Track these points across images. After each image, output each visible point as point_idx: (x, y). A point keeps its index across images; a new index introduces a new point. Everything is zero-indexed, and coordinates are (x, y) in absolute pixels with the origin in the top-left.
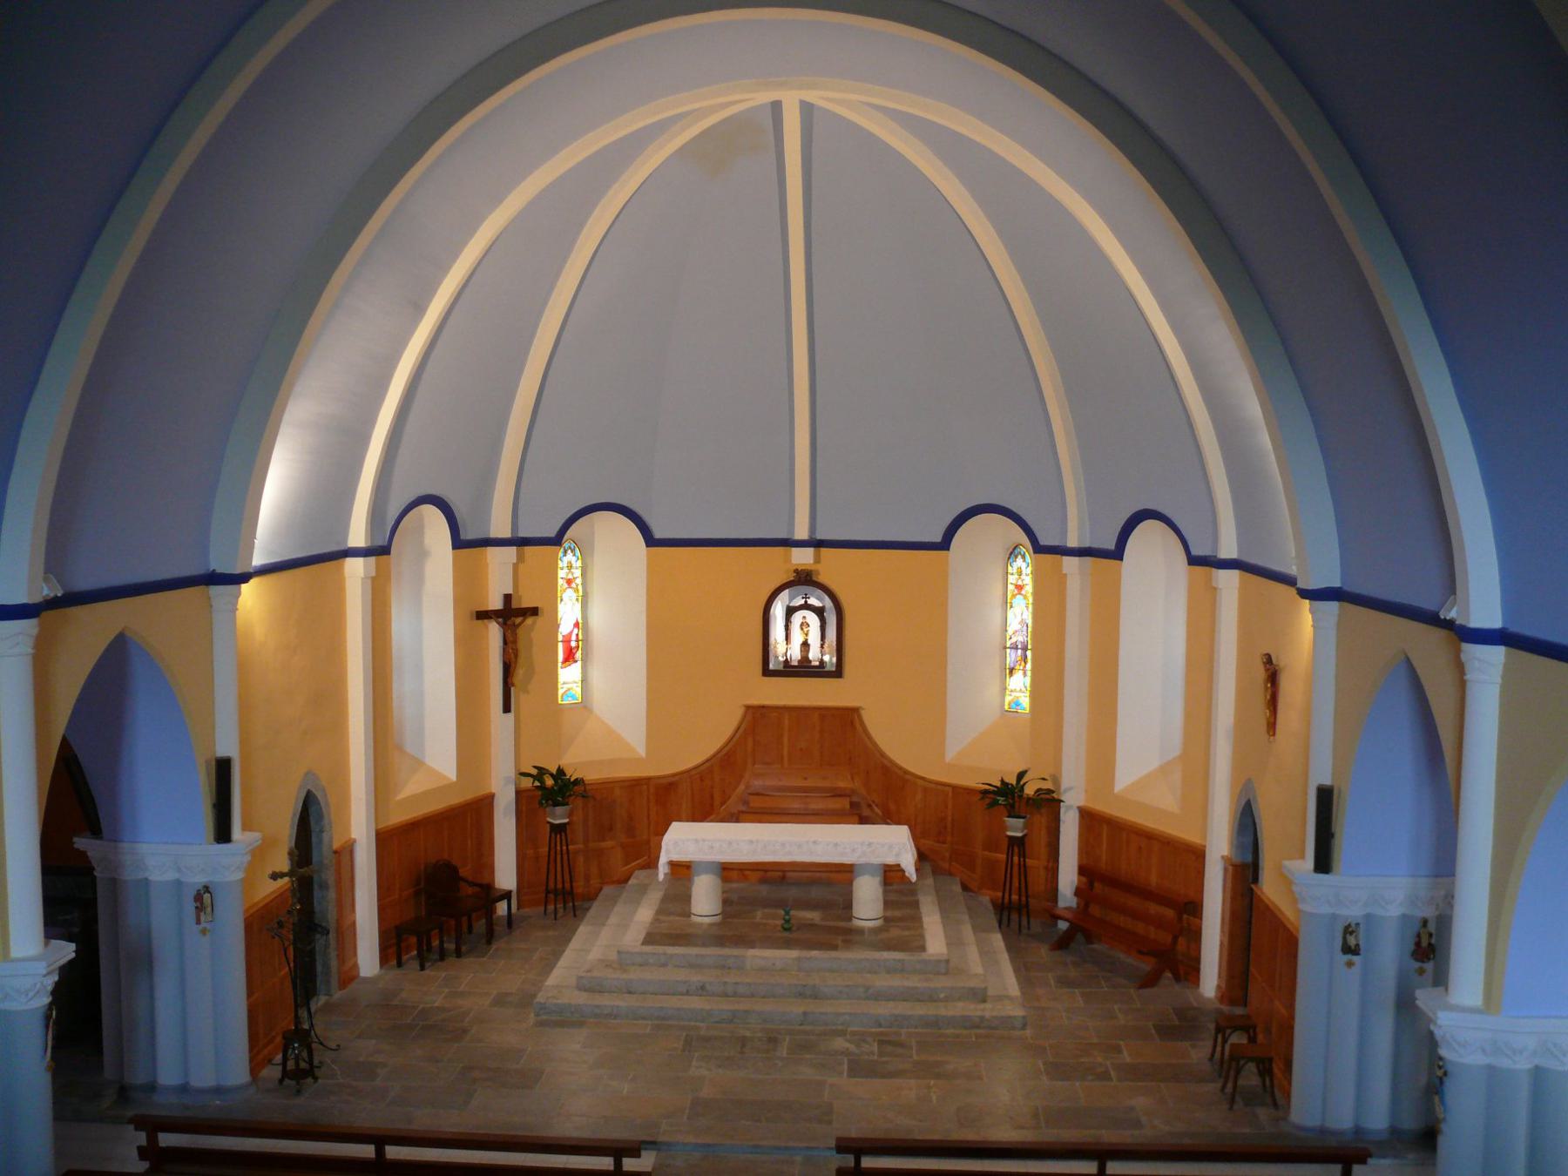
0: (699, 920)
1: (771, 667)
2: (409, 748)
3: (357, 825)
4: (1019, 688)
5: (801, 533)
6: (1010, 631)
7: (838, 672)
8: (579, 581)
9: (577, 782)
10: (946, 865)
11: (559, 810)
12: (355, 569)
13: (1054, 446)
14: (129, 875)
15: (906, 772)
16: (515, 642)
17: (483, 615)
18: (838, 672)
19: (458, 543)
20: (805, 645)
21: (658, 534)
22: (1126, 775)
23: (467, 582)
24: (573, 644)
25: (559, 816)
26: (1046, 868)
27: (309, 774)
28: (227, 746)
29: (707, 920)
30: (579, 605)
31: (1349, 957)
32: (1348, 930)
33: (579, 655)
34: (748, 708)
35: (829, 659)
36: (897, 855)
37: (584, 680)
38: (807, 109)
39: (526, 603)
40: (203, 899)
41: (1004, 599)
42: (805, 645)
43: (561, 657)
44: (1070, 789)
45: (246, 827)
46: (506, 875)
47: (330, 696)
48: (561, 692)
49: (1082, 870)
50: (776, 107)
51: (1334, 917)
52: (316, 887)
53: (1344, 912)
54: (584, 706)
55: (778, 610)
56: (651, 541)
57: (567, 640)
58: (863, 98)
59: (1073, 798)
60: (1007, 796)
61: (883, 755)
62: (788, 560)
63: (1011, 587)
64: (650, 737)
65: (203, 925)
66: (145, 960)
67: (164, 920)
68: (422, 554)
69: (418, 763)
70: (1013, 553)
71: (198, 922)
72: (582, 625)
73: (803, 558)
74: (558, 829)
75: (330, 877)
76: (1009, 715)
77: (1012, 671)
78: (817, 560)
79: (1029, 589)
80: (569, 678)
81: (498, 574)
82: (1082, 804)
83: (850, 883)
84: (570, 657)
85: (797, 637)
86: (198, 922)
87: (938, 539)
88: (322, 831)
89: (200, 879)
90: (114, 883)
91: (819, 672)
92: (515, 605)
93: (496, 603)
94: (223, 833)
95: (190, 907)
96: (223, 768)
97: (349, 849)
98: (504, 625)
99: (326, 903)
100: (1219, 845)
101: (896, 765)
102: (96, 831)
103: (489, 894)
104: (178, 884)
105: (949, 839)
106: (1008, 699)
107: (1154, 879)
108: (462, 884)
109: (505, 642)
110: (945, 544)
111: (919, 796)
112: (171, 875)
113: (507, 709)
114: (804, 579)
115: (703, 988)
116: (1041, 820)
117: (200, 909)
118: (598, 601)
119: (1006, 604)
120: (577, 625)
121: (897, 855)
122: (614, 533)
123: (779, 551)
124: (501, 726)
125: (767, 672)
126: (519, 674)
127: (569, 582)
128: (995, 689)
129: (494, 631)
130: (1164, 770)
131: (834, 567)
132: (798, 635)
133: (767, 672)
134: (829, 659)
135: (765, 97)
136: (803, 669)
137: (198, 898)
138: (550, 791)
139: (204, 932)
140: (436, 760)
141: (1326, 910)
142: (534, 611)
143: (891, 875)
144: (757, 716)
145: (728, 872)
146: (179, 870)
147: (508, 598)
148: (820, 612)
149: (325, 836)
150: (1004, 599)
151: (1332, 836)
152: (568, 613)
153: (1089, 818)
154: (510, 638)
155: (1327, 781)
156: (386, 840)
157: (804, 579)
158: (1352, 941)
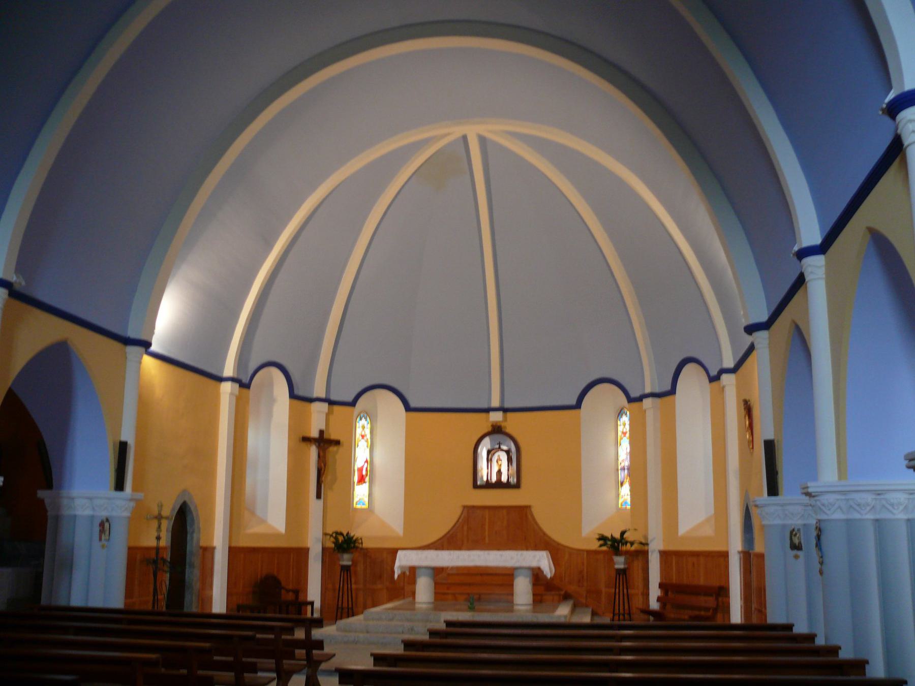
0: (420, 606)
1: (479, 483)
2: (259, 513)
3: (217, 536)
4: (625, 492)
5: (495, 403)
6: (620, 459)
7: (517, 486)
8: (368, 436)
9: (357, 539)
10: (584, 601)
11: (346, 556)
12: (227, 388)
13: (634, 334)
14: (66, 512)
15: (559, 544)
16: (325, 457)
17: (306, 440)
18: (517, 486)
19: (293, 395)
20: (499, 473)
21: (413, 404)
22: (684, 528)
23: (297, 421)
24: (364, 473)
25: (346, 560)
26: (643, 594)
27: (185, 491)
28: (128, 434)
29: (424, 606)
30: (368, 450)
31: (795, 552)
32: (792, 533)
33: (367, 479)
34: (464, 507)
35: (513, 480)
36: (539, 561)
37: (370, 495)
38: (483, 140)
39: (334, 436)
40: (104, 526)
41: (614, 441)
42: (499, 473)
43: (356, 479)
44: (654, 538)
45: (135, 489)
46: (314, 592)
47: (207, 455)
48: (356, 500)
49: (661, 586)
50: (465, 138)
51: (784, 526)
52: (187, 566)
53: (789, 522)
54: (370, 509)
55: (483, 452)
56: (408, 408)
57: (360, 470)
58: (510, 128)
59: (656, 547)
60: (614, 544)
61: (545, 534)
62: (488, 418)
63: (620, 434)
64: (405, 529)
65: (103, 542)
66: (68, 565)
67: (81, 538)
68: (272, 401)
69: (263, 521)
70: (620, 413)
71: (100, 539)
72: (371, 462)
73: (496, 417)
74: (345, 569)
75: (197, 561)
76: (620, 511)
77: (622, 484)
78: (505, 419)
79: (628, 435)
80: (361, 493)
81: (317, 419)
82: (662, 548)
83: (513, 581)
84: (362, 480)
85: (495, 469)
86: (100, 539)
87: (573, 402)
88: (193, 532)
89: (104, 514)
90: (58, 518)
91: (508, 485)
92: (326, 436)
93: (315, 434)
94: (119, 485)
95: (97, 529)
96: (123, 448)
97: (208, 551)
98: (319, 447)
99: (193, 575)
100: (735, 545)
101: (554, 541)
102: (49, 485)
103: (302, 604)
104: (92, 518)
105: (585, 584)
106: (621, 501)
107: (702, 582)
108: (283, 591)
109: (319, 456)
110: (578, 405)
111: (566, 557)
112: (88, 512)
113: (319, 496)
114: (497, 430)
115: (412, 629)
116: (637, 565)
117: (102, 531)
118: (375, 446)
119: (617, 444)
120: (367, 461)
121: (539, 561)
122: (388, 404)
123: (483, 415)
124: (315, 507)
125: (475, 486)
126: (327, 478)
127: (363, 437)
128: (613, 494)
129: (313, 451)
130: (708, 520)
131: (513, 423)
132: (495, 466)
133: (475, 486)
134: (513, 480)
135: (457, 131)
136: (499, 485)
137: (102, 525)
138: (343, 544)
139: (103, 546)
140: (272, 519)
141: (778, 522)
142: (337, 443)
143: (536, 575)
144: (470, 511)
145: (437, 572)
146: (93, 509)
147: (321, 432)
148: (508, 452)
149: (195, 535)
150: (614, 441)
151: (777, 473)
152: (361, 454)
153: (665, 555)
154: (322, 454)
155: (770, 436)
156: (234, 553)
157: (497, 430)
158: (796, 541)
